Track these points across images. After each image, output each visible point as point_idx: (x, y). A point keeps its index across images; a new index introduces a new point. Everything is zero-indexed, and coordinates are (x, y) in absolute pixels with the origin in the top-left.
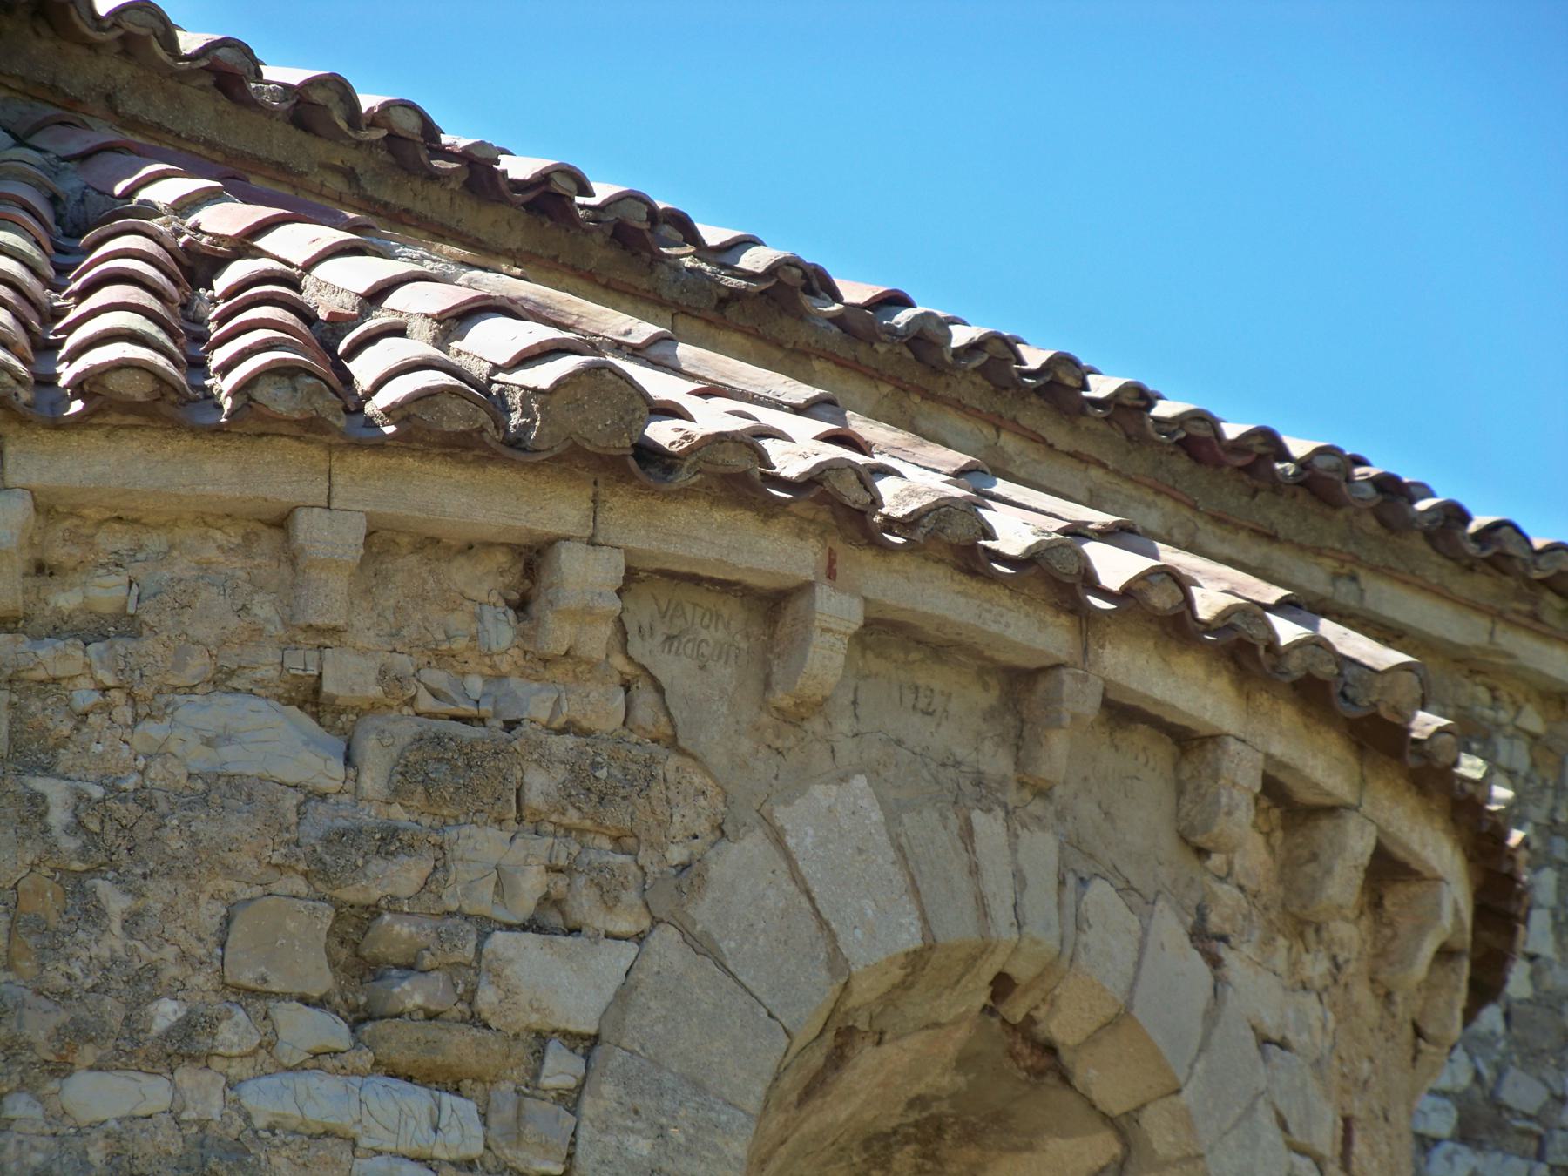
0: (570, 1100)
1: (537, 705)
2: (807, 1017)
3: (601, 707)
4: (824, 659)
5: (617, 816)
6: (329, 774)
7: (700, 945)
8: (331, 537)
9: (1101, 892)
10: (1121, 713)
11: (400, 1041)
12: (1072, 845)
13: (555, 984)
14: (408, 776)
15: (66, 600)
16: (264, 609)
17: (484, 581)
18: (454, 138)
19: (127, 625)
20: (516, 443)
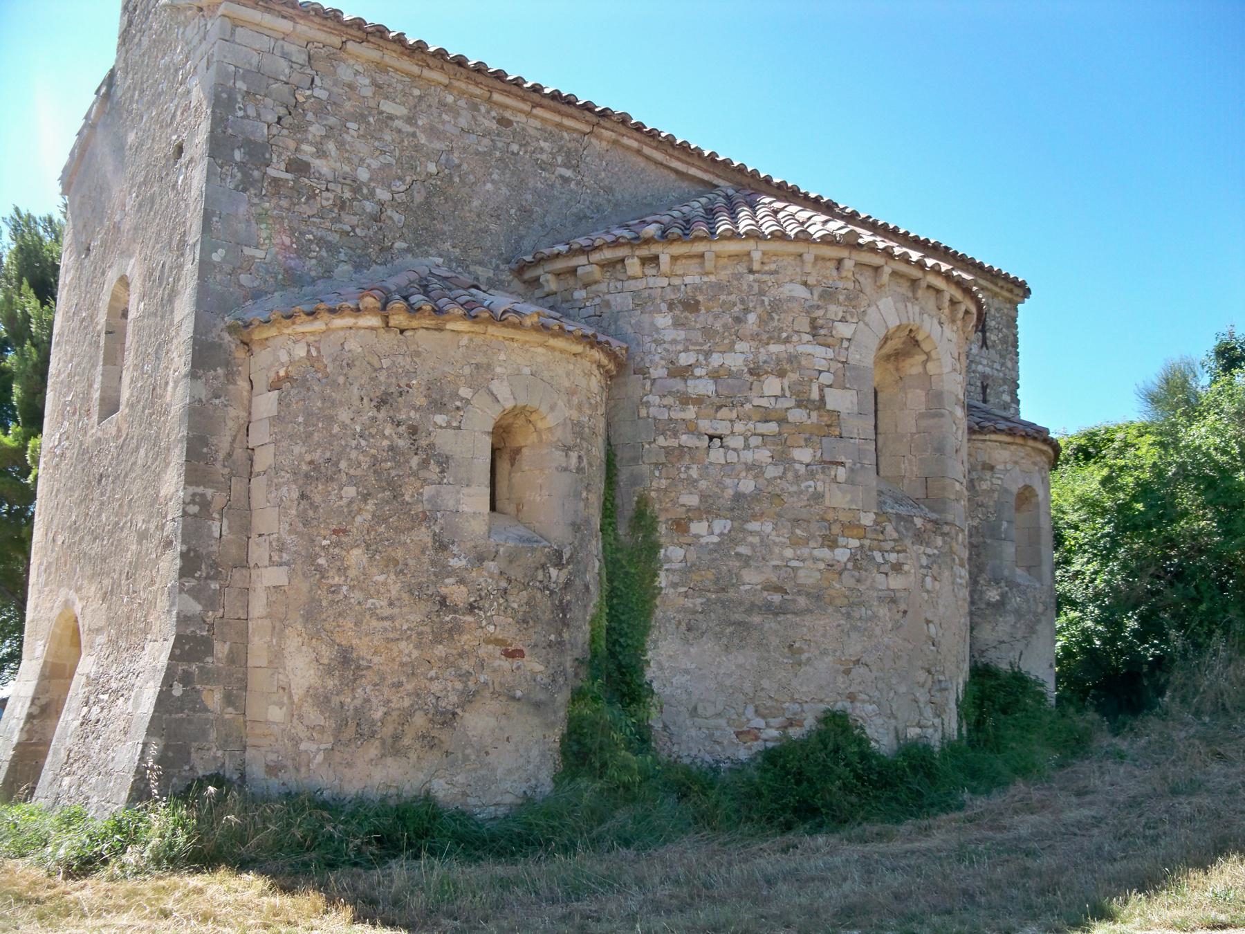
0: (847, 349)
1: (841, 285)
2: (882, 336)
3: (850, 285)
4: (885, 278)
5: (854, 303)
6: (808, 296)
7: (866, 324)
8: (809, 258)
9: (925, 316)
10: (929, 287)
11: (820, 339)
12: (921, 308)
13: (844, 330)
14: (821, 297)
15: (766, 268)
16: (798, 269)
17: (832, 265)
18: (802, 191)
19: (776, 272)
20: (838, 242)
